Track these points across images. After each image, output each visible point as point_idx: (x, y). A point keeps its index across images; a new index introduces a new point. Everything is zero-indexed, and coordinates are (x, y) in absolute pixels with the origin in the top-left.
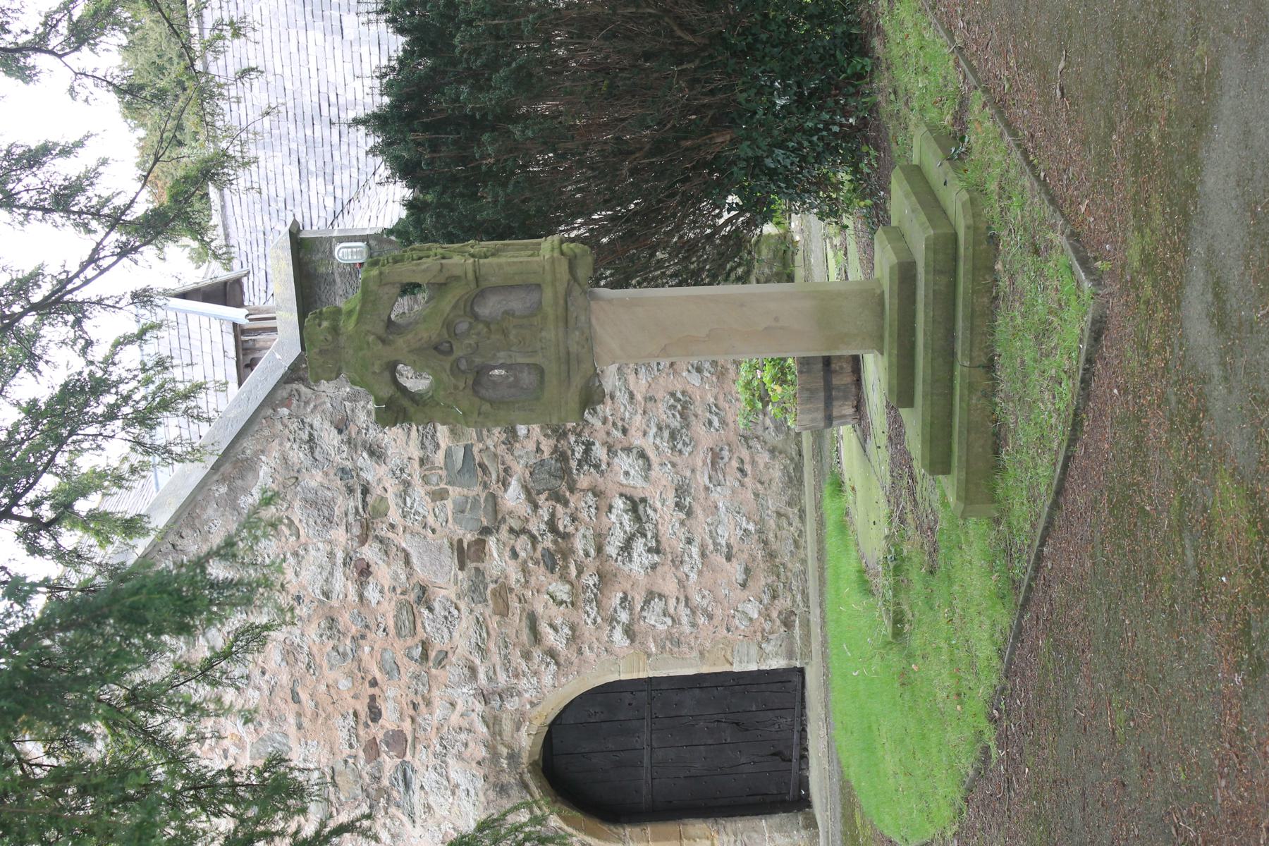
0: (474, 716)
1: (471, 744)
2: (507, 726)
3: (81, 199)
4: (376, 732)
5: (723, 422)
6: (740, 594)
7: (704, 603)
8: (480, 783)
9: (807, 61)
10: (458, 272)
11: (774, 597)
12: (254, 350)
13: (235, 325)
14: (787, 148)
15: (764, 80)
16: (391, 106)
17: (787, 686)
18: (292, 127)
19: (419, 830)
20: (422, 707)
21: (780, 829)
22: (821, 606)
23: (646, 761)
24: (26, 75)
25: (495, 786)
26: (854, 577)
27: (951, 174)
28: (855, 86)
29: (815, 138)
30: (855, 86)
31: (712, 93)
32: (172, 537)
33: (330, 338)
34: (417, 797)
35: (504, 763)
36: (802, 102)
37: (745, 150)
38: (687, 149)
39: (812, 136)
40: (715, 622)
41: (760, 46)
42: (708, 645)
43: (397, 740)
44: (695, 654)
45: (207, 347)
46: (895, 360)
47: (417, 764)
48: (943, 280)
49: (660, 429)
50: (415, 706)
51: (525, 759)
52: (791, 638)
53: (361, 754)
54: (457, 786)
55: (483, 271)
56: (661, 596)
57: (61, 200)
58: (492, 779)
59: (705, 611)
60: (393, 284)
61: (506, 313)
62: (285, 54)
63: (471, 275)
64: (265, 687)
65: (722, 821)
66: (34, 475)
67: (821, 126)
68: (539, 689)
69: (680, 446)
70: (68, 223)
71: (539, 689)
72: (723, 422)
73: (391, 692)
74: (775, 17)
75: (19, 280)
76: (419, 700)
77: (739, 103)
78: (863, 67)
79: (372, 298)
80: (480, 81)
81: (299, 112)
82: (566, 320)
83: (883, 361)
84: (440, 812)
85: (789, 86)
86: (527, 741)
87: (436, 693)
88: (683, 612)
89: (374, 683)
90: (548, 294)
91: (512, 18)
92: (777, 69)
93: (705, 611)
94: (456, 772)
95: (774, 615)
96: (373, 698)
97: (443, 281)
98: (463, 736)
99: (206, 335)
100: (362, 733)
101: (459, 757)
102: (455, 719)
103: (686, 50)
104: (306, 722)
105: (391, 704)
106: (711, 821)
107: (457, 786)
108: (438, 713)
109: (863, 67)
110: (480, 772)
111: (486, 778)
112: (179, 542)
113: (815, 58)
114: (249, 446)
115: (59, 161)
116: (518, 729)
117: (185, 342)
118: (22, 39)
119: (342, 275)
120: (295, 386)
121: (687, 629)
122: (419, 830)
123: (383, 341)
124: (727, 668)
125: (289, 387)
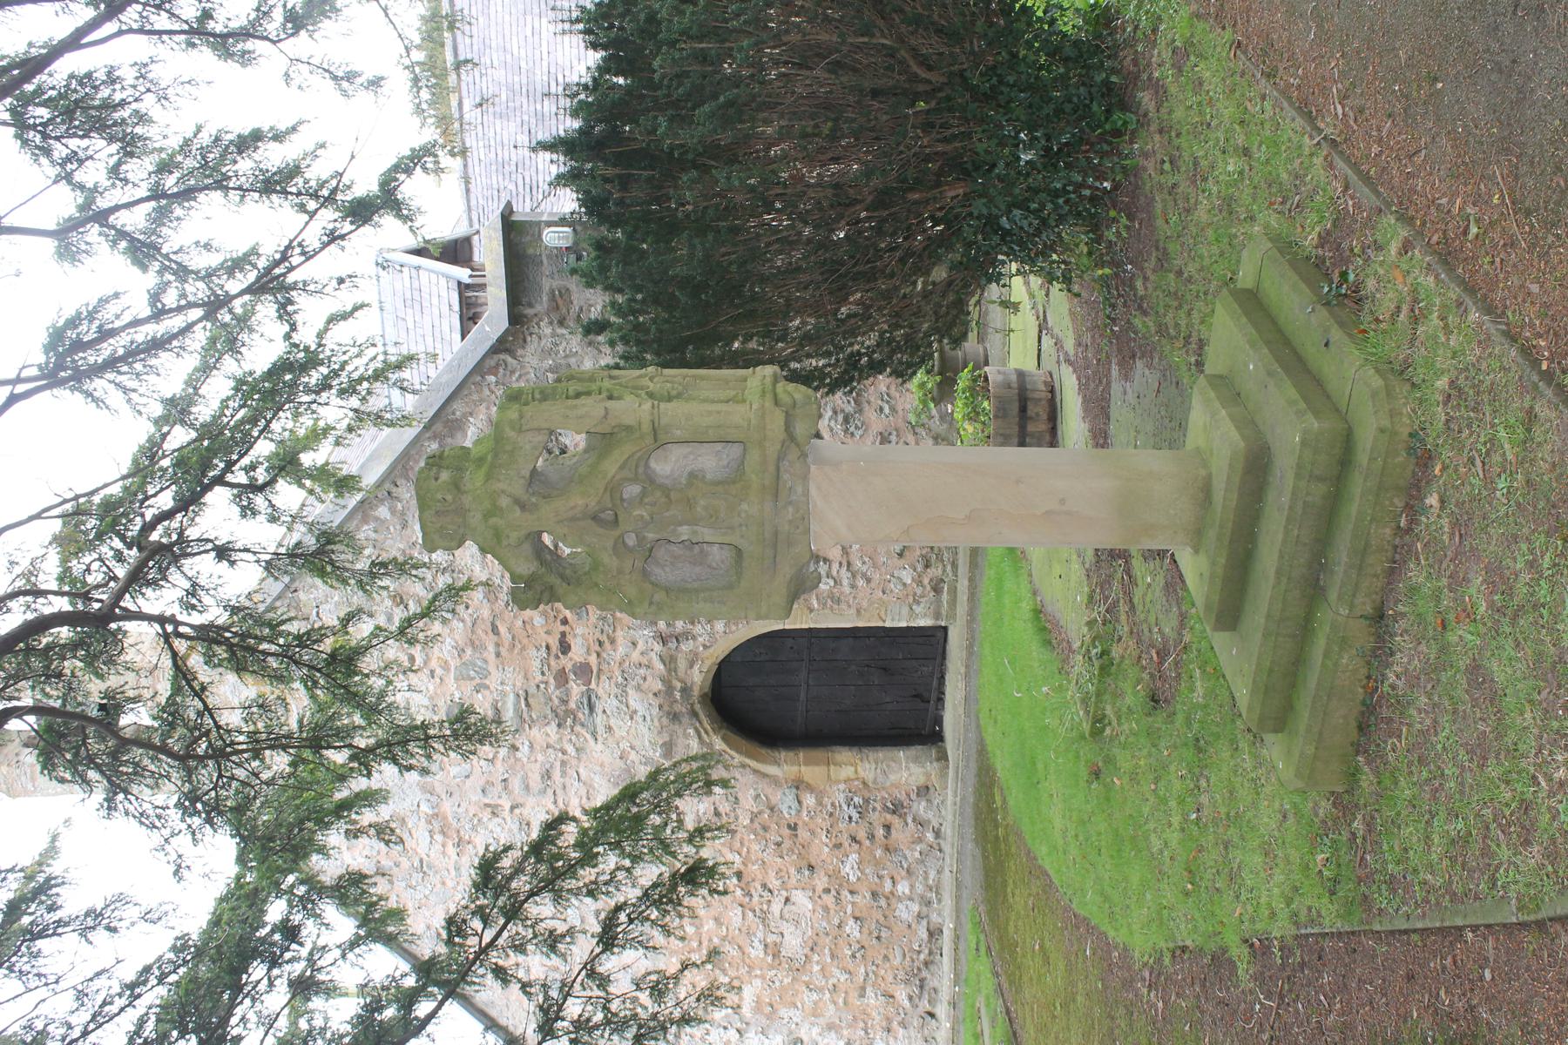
0: (653, 655)
1: (649, 679)
2: (682, 664)
3: (299, 181)
4: (566, 662)
5: (893, 410)
6: (896, 561)
7: (864, 569)
8: (655, 711)
9: (1059, 111)
10: (629, 420)
11: (927, 566)
12: (476, 305)
13: (459, 283)
14: (1028, 209)
15: (1008, 130)
16: (581, 131)
17: (930, 643)
18: (525, 101)
19: (600, 747)
20: (607, 644)
21: (916, 760)
22: (970, 580)
23: (802, 696)
24: (246, 58)
25: (669, 713)
26: (1028, 615)
27: (1336, 334)
28: (1110, 143)
29: (1061, 201)
30: (1110, 143)
31: (946, 140)
32: (387, 486)
33: (449, 498)
34: (599, 719)
35: (678, 695)
36: (1050, 158)
37: (979, 207)
38: (916, 202)
39: (1058, 197)
40: (873, 585)
41: (1005, 89)
42: (865, 604)
43: (583, 671)
44: (853, 611)
45: (435, 301)
46: (1220, 571)
47: (600, 692)
48: (1320, 490)
49: (835, 412)
50: (601, 644)
51: (696, 692)
52: (939, 602)
53: (552, 681)
54: (635, 712)
55: (664, 421)
56: (825, 560)
57: (273, 184)
58: (666, 708)
59: (864, 575)
60: (539, 430)
61: (692, 475)
62: (522, 37)
63: (646, 427)
64: (468, 620)
65: (865, 750)
66: (248, 444)
67: (1070, 188)
68: (712, 635)
69: (852, 429)
70: (286, 204)
71: (712, 635)
72: (893, 410)
73: (579, 631)
74: (1025, 57)
75: (233, 260)
76: (604, 638)
77: (977, 154)
78: (1125, 123)
79: (508, 448)
80: (681, 114)
81: (531, 89)
82: (775, 491)
83: (1203, 562)
84: (620, 733)
85: (1036, 138)
86: (699, 677)
87: (619, 634)
88: (845, 574)
89: (565, 622)
90: (754, 456)
91: (723, 41)
92: (1023, 118)
93: (864, 575)
94: (634, 700)
95: (926, 581)
96: (563, 634)
97: (608, 430)
98: (642, 671)
99: (434, 289)
100: (553, 663)
101: (638, 688)
102: (635, 656)
103: (921, 88)
104: (504, 651)
105: (579, 640)
106: (855, 749)
107: (635, 712)
108: (621, 650)
109: (1125, 123)
110: (656, 702)
111: (660, 707)
112: (394, 490)
113: (1068, 107)
114: (459, 408)
115: (273, 145)
116: (691, 667)
117: (416, 293)
118: (235, 25)
119: (549, 257)
120: (502, 356)
121: (847, 590)
122: (600, 747)
123: (523, 507)
124: (880, 624)
125: (496, 357)
